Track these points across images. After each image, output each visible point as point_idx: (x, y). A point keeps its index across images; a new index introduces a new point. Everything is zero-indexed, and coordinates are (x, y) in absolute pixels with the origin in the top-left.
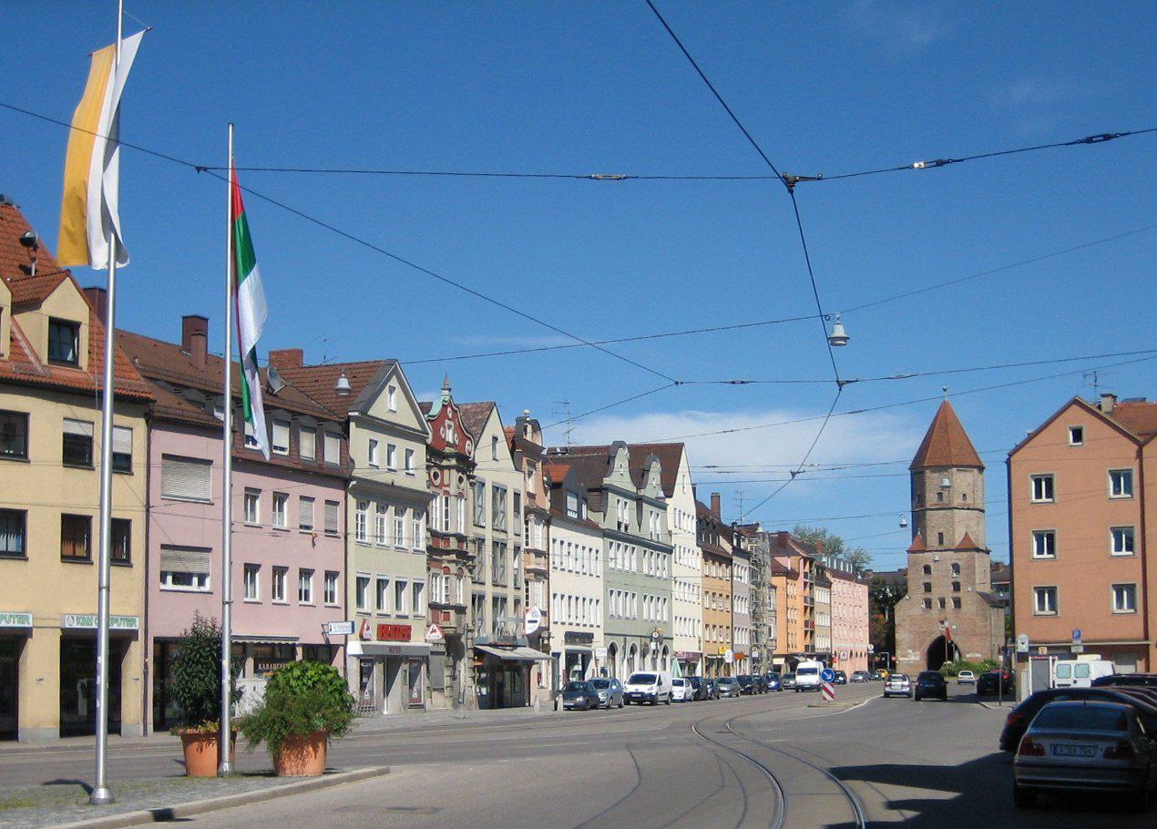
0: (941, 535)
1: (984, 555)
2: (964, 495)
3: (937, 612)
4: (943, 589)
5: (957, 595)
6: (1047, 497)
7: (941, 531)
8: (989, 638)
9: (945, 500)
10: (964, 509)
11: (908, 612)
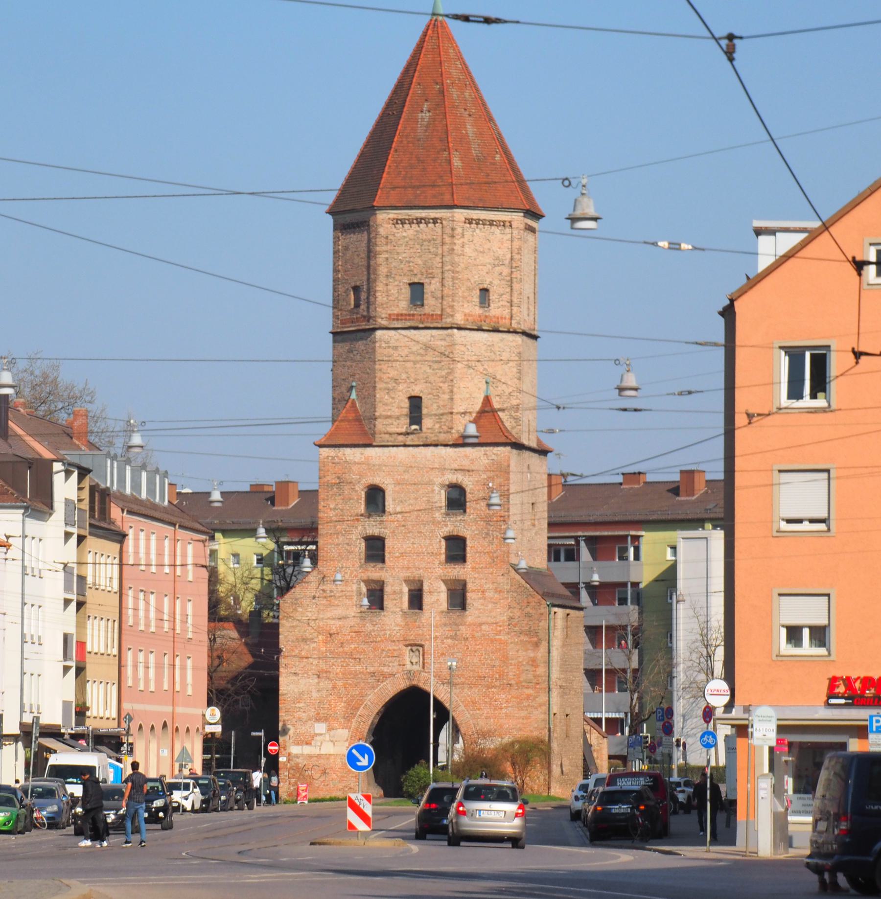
0: (415, 402)
1: (534, 459)
2: (485, 291)
3: (399, 619)
4: (415, 553)
5: (456, 571)
6: (814, 396)
7: (416, 391)
8: (543, 698)
9: (431, 305)
10: (480, 329)
11: (318, 622)
